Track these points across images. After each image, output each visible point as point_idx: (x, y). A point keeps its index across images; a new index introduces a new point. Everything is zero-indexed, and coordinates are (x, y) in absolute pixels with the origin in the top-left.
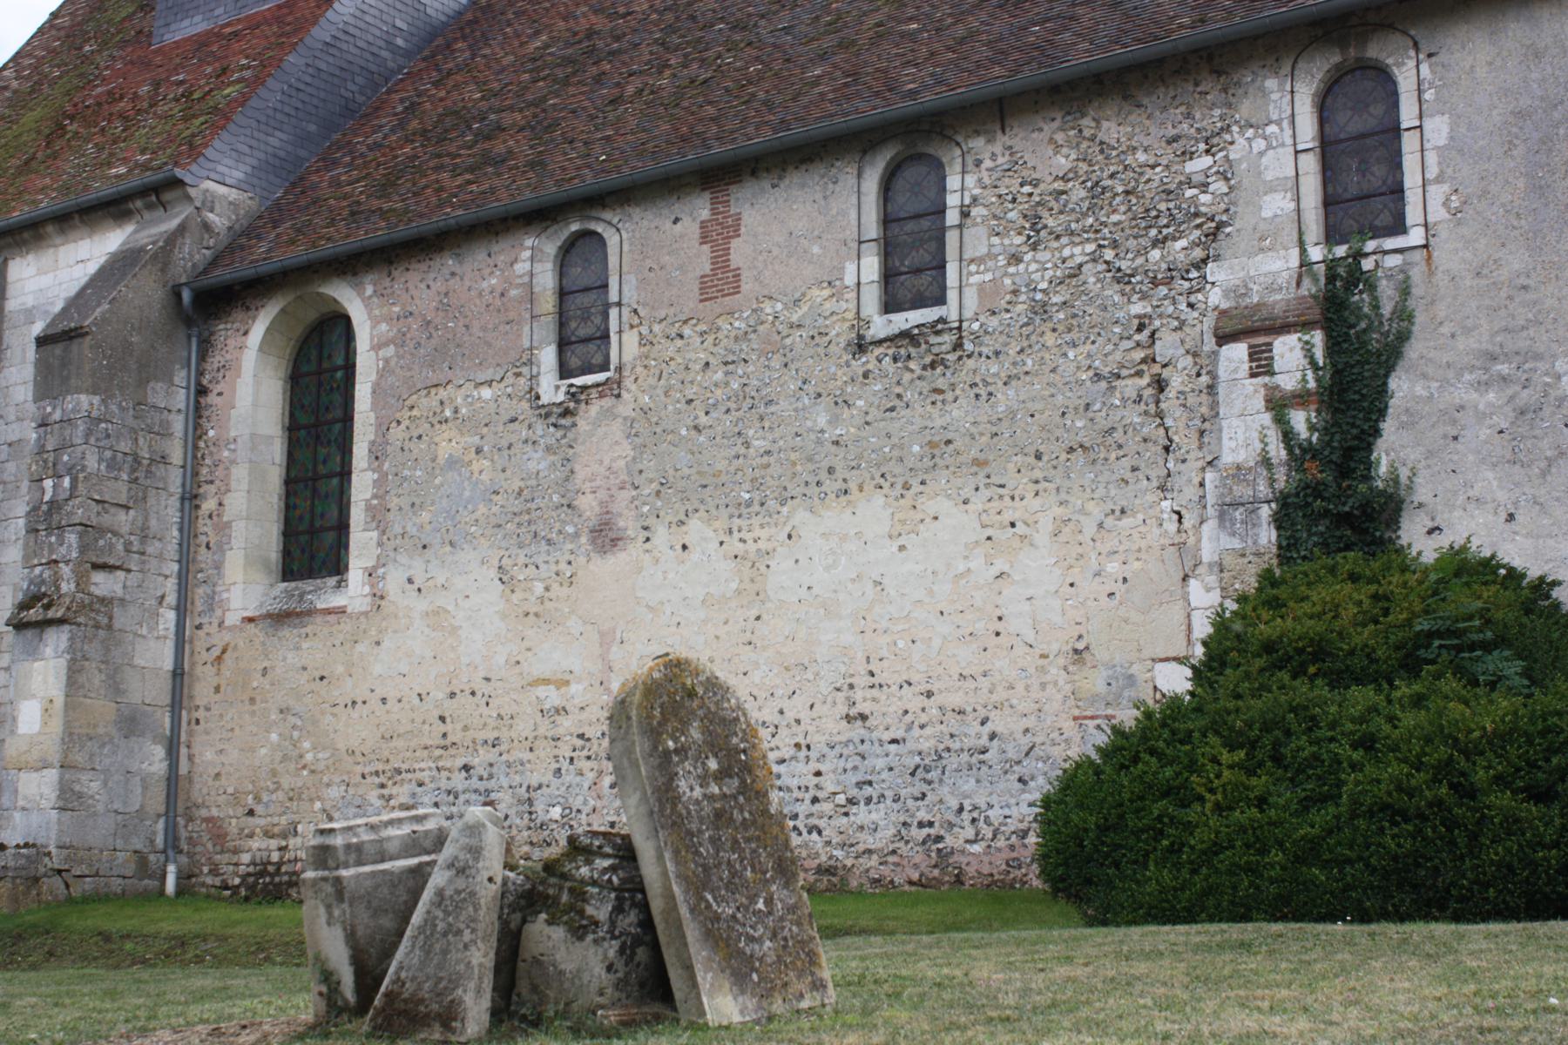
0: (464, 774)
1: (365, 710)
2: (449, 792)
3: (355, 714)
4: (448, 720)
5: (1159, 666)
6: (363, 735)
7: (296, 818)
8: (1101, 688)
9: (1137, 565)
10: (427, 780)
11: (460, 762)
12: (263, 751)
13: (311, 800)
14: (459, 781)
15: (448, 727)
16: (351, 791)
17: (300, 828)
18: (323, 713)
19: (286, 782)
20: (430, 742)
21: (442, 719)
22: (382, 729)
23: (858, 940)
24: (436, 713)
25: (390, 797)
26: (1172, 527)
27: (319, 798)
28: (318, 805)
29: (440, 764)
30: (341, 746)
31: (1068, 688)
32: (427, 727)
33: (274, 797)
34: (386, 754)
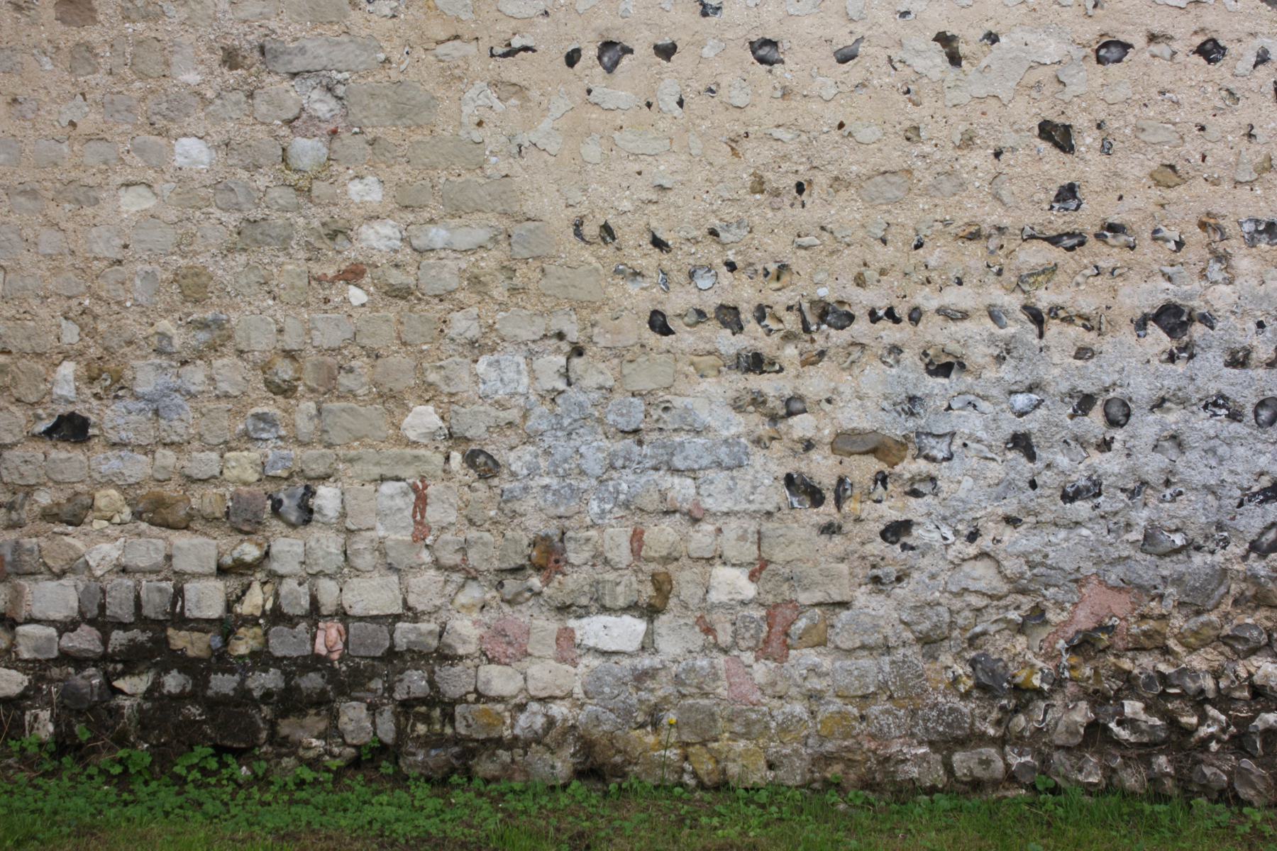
0: (1158, 339)
1: (670, 81)
2: (1085, 403)
3: (620, 91)
4: (1087, 140)
6: (662, 170)
7: (313, 459)
10: (979, 354)
11: (1146, 294)
12: (133, 203)
13: (392, 399)
14: (1136, 362)
15: (1086, 165)
16: (593, 373)
17: (327, 497)
18: (454, 77)
19: (257, 325)
20: (991, 216)
21: (1057, 135)
22: (757, 154)
23: (600, 646)
24: (1028, 114)
25: (793, 406)
27: (428, 392)
28: (422, 419)
29: (1044, 299)
30: (549, 204)
32: (979, 158)
33: (196, 376)
34: (778, 246)
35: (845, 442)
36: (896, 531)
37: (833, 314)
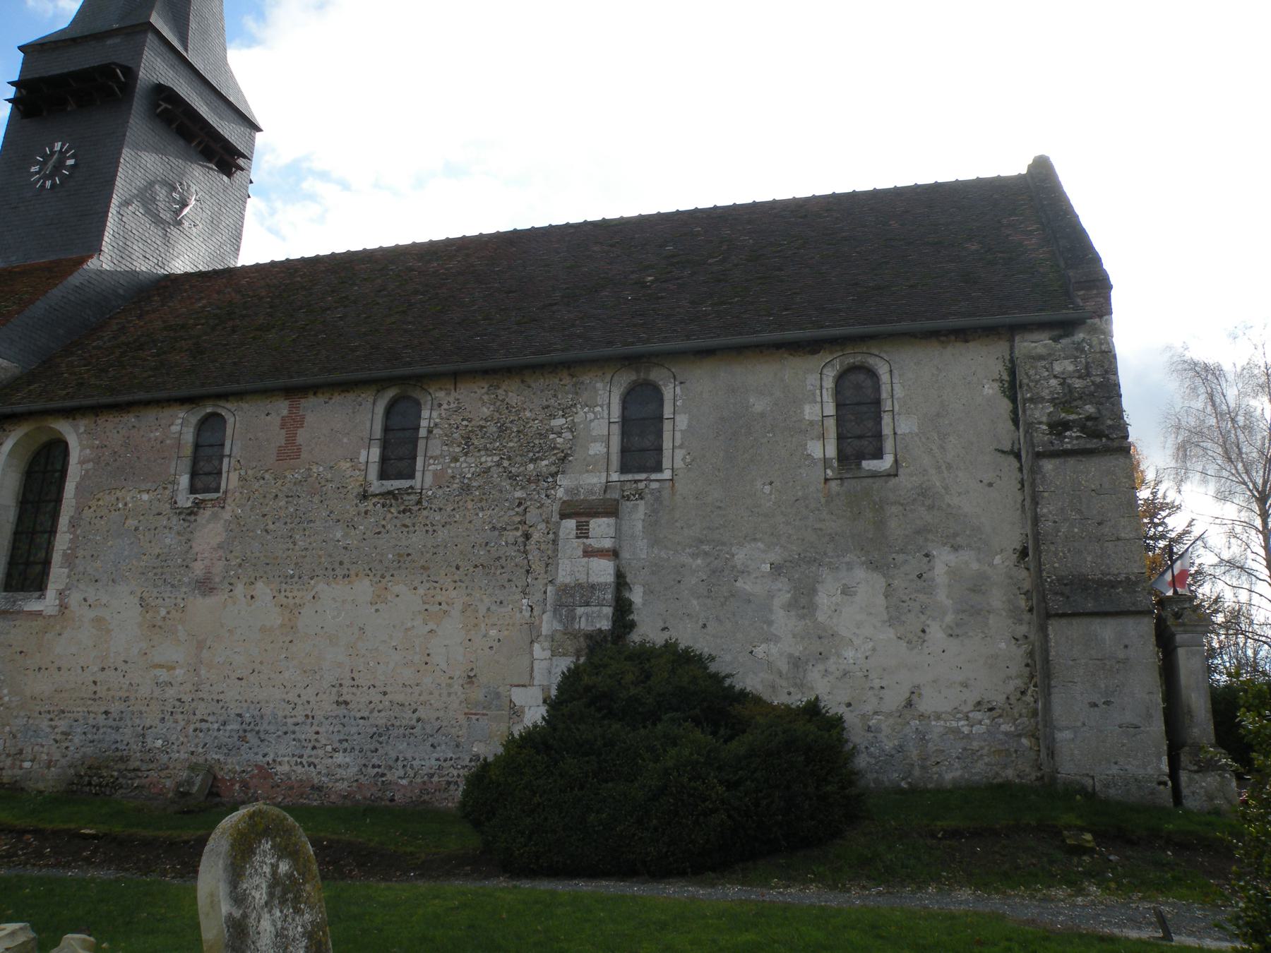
5: (514, 689)
8: (481, 697)
9: (506, 633)
15: (98, 688)
24: (92, 679)
26: (527, 614)
28: (7, 728)
31: (463, 697)
35: (63, 733)
36: (67, 748)
37: (63, 712)
